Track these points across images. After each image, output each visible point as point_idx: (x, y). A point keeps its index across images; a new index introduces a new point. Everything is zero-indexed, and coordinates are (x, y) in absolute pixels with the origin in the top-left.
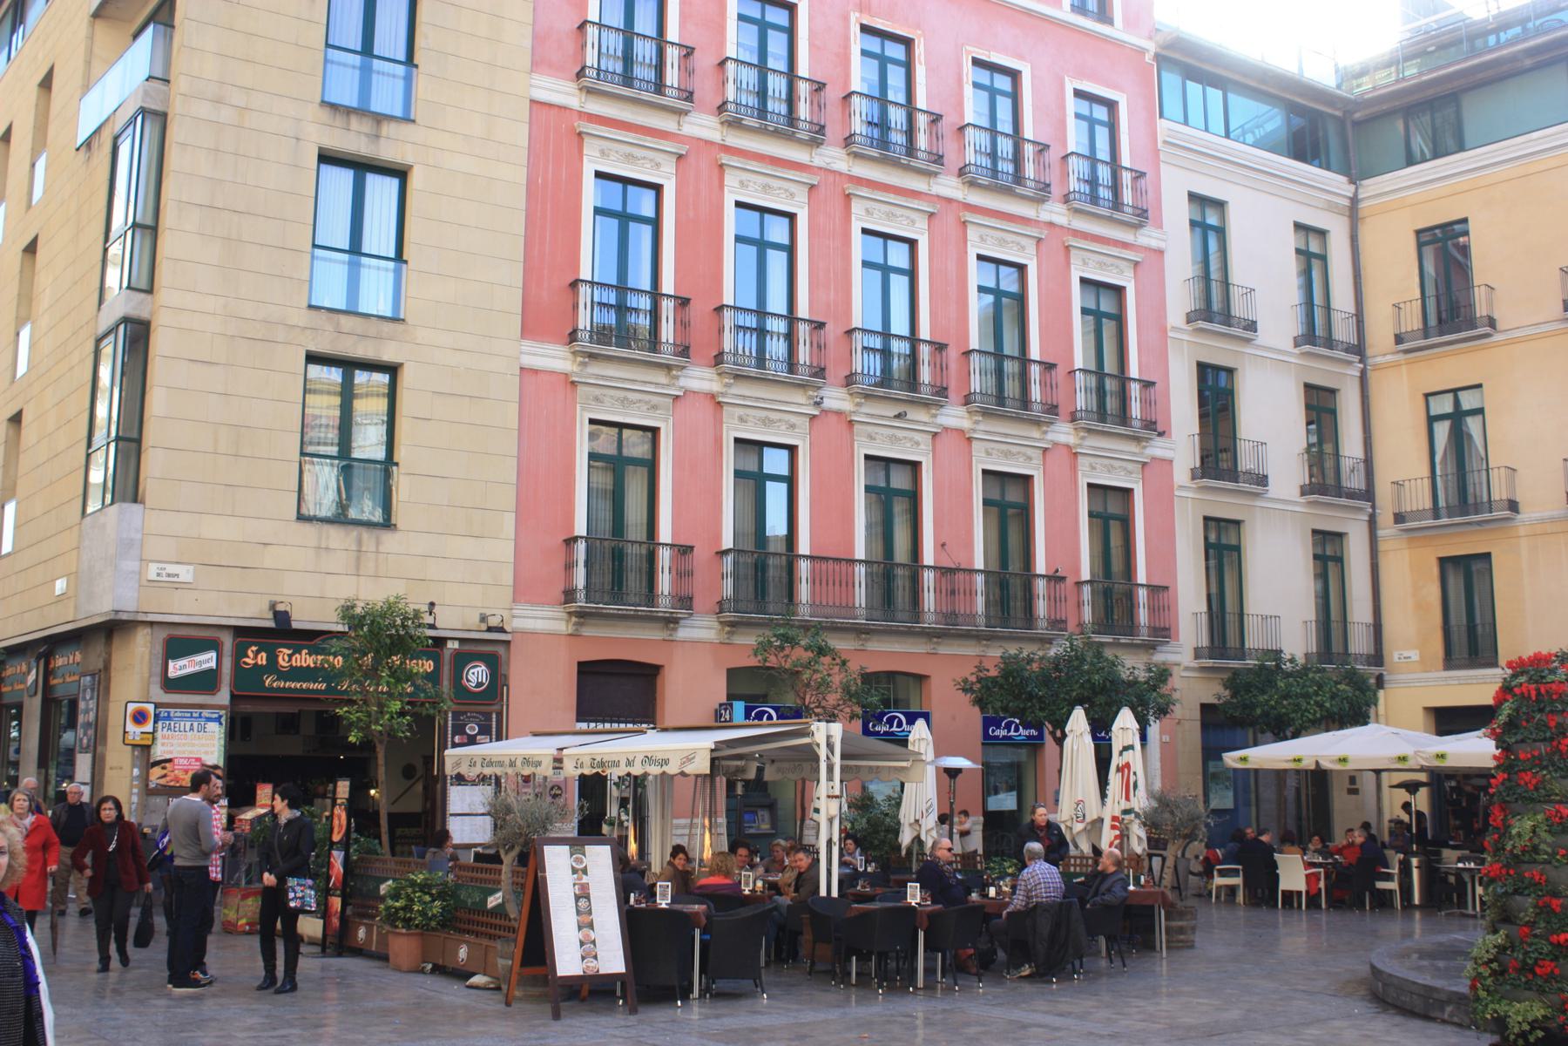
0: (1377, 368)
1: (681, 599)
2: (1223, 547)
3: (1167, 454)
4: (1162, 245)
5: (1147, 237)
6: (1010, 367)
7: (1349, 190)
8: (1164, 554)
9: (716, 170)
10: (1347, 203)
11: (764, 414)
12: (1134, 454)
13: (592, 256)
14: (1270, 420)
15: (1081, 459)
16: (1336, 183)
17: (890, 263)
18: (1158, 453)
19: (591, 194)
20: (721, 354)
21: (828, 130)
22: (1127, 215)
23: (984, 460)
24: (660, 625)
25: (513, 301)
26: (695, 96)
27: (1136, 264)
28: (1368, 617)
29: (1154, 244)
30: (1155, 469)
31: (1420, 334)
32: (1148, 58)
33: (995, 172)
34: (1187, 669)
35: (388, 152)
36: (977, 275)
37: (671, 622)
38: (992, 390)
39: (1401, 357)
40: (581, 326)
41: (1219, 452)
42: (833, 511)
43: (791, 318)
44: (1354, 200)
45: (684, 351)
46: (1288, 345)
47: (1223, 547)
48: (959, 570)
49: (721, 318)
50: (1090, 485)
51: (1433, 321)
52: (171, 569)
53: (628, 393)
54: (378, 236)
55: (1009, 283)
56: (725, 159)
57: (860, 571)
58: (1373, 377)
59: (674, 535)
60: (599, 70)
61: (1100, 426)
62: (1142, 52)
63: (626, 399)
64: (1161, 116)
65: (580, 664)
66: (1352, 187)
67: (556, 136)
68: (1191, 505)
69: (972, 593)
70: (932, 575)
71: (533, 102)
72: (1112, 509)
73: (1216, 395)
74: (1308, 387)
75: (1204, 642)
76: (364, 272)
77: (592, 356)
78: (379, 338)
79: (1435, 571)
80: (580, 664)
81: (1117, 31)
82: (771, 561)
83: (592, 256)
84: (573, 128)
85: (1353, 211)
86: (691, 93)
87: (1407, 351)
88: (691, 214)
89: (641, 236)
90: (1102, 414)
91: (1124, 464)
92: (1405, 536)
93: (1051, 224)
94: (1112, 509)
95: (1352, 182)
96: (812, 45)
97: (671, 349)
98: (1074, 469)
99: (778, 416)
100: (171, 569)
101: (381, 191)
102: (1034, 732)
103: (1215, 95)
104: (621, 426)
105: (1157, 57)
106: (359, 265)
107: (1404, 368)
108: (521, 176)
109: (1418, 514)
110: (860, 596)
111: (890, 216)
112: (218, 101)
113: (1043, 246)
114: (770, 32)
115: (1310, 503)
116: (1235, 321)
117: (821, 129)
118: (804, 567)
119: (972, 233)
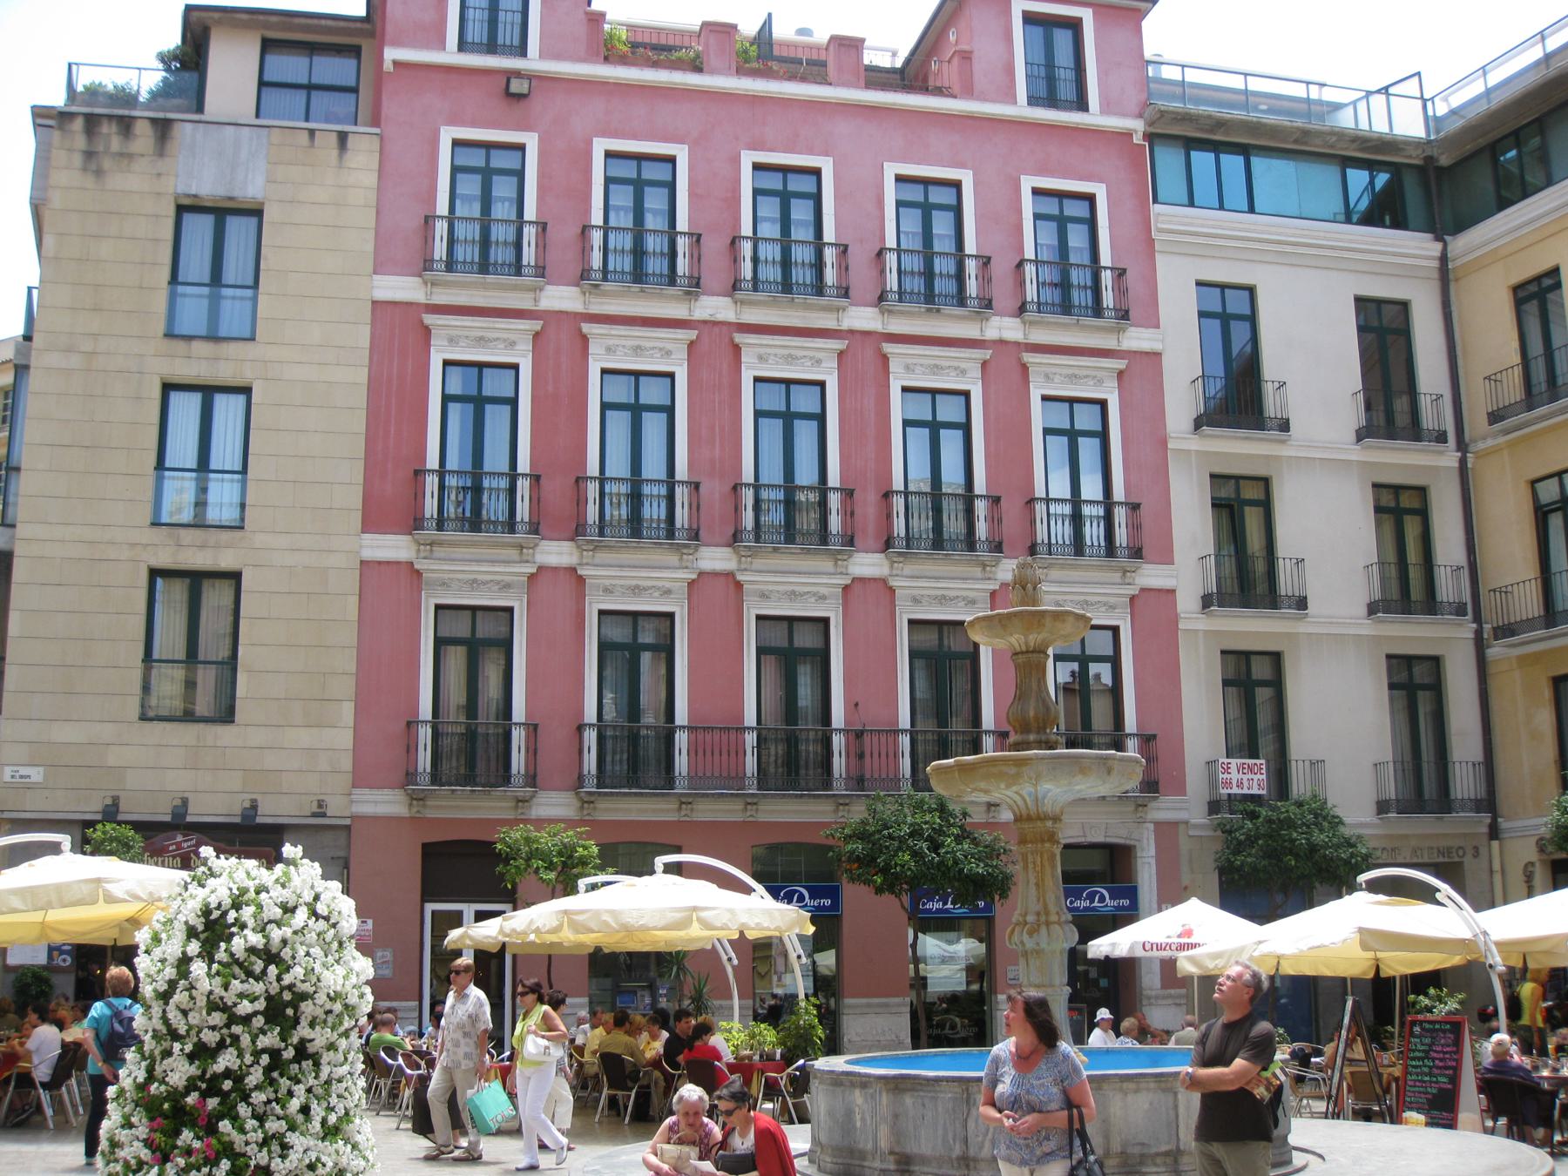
2: (1255, 686)
10: (1436, 264)
13: (438, 439)
14: (1326, 533)
16: (1416, 246)
19: (1038, 417)
25: (355, 498)
26: (851, 293)
28: (1477, 754)
29: (1146, 346)
30: (1154, 608)
32: (1138, 139)
34: (1196, 826)
35: (224, 373)
39: (1502, 440)
41: (1249, 575)
42: (557, 675)
43: (442, 473)
44: (1444, 259)
49: (1032, 512)
52: (24, 771)
53: (476, 573)
54: (225, 452)
60: (1039, 304)
62: (1128, 135)
64: (1155, 201)
65: (424, 846)
66: (1439, 246)
67: (400, 332)
68: (1204, 635)
71: (374, 303)
73: (1241, 506)
76: (166, 482)
78: (217, 546)
79: (1547, 693)
80: (424, 846)
81: (1094, 117)
82: (643, 732)
83: (438, 439)
85: (1445, 274)
88: (550, 388)
89: (805, 433)
93: (1002, 342)
95: (1439, 238)
96: (692, 194)
99: (643, 580)
100: (24, 771)
101: (227, 410)
102: (827, 902)
103: (1233, 164)
105: (1149, 137)
106: (207, 480)
108: (362, 376)
109: (1529, 624)
112: (69, 350)
114: (1070, 226)
116: (1269, 424)
118: (681, 739)
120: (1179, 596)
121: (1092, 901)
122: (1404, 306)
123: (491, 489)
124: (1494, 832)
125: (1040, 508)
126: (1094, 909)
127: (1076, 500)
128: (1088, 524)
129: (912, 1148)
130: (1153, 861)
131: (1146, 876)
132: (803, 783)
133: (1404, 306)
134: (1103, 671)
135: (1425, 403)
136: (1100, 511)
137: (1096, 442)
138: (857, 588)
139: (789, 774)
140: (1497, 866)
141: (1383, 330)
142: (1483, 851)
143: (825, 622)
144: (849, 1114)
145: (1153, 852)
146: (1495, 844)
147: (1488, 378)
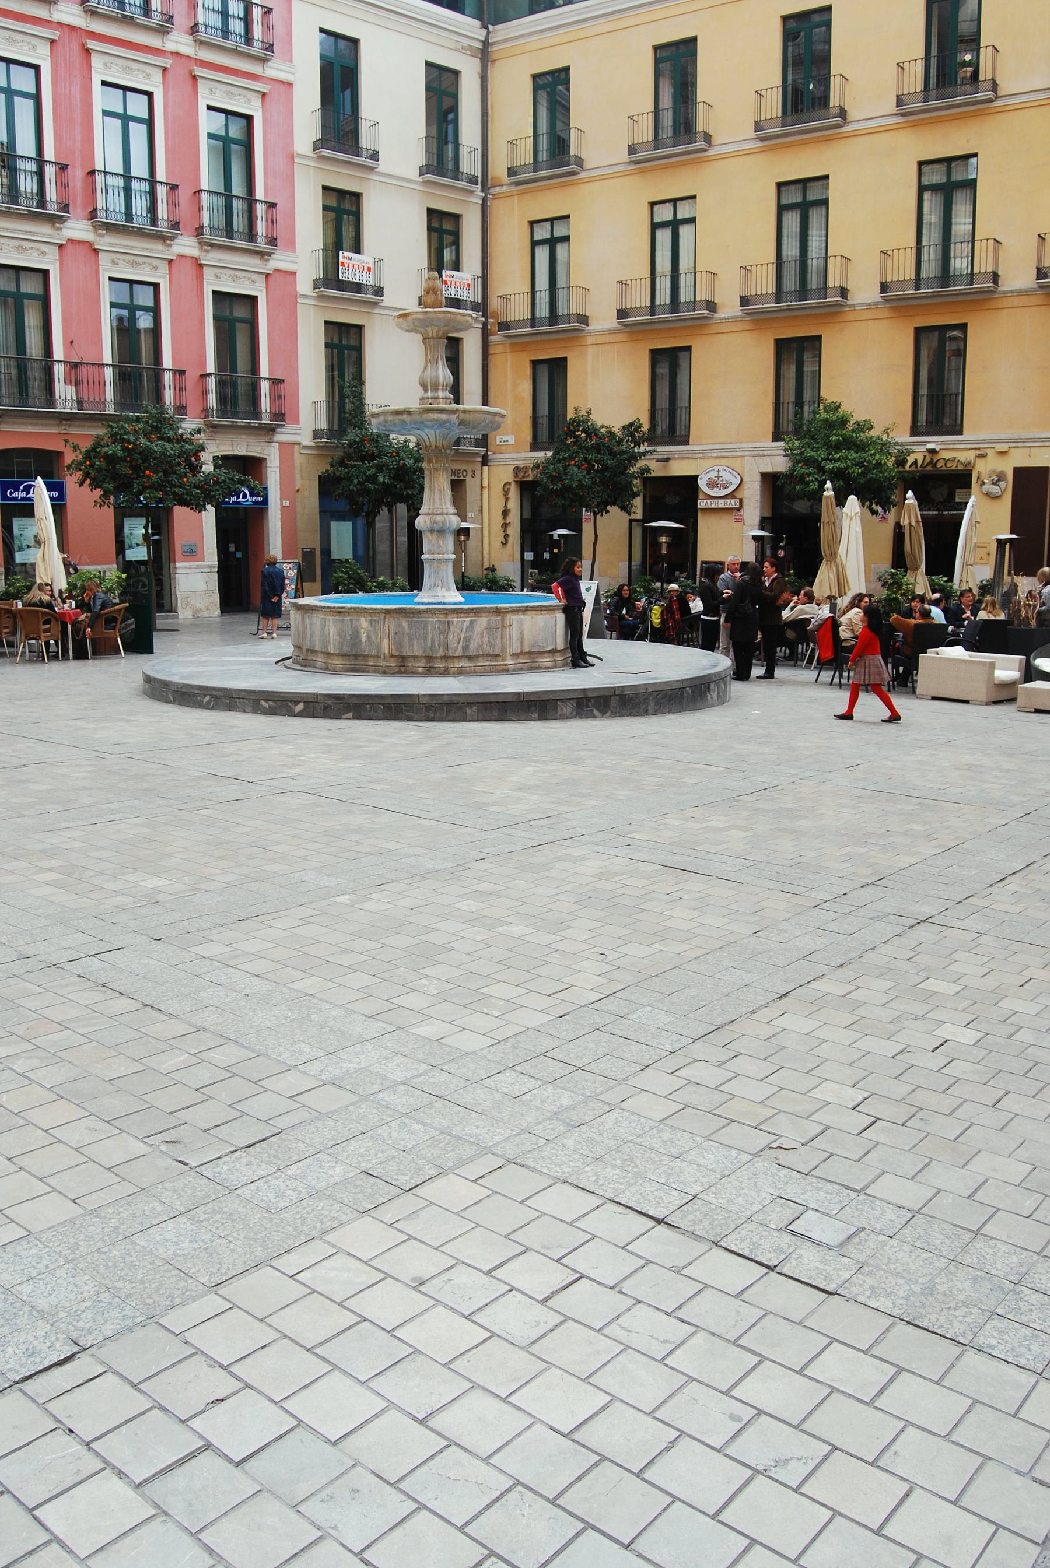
0: (495, 197)
1: (275, 415)
2: (345, 347)
3: (290, 267)
4: (289, 78)
5: (274, 70)
6: (237, 206)
7: (481, 34)
8: (287, 353)
9: (189, 81)
10: (480, 46)
11: (131, 258)
12: (50, 236)
15: (206, 270)
16: (467, 25)
17: (129, 113)
18: (283, 266)
19: (101, 99)
20: (95, 210)
21: (175, 20)
22: (257, 49)
23: (212, 283)
24: (264, 432)
27: (264, 95)
31: (531, 167)
33: (225, 33)
34: (306, 447)
36: (101, 99)
37: (271, 430)
38: (222, 224)
39: (513, 188)
40: (99, 207)
44: (486, 43)
45: (175, 225)
46: (413, 174)
47: (345, 347)
48: (81, 363)
49: (199, 200)
50: (214, 292)
51: (543, 156)
55: (235, 131)
56: (198, 71)
57: (108, 373)
58: (495, 206)
59: (270, 372)
61: (227, 242)
63: (20, 247)
66: (484, 32)
69: (102, 384)
70: (267, 384)
72: (235, 315)
74: (431, 212)
75: (324, 425)
77: (212, 245)
79: (528, 371)
82: (240, 381)
84: (191, 72)
85: (485, 54)
86: (172, 17)
87: (518, 184)
90: (229, 233)
91: (248, 275)
92: (509, 341)
94: (235, 315)
97: (165, 224)
98: (200, 278)
102: (260, 499)
104: (132, 282)
107: (516, 197)
110: (109, 392)
111: (128, 70)
113: (170, 75)
115: (321, 297)
117: (170, 19)
119: (96, 61)
120: (299, 277)
121: (28, 493)
122: (456, 73)
123: (25, 171)
124: (485, 461)
125: (99, 178)
126: (239, 503)
127: (128, 177)
128: (22, 177)
129: (406, 652)
130: (278, 470)
131: (273, 480)
132: (31, 402)
133: (456, 73)
134: (144, 321)
135: (464, 152)
136: (145, 187)
137: (30, 103)
138: (70, 248)
139: (21, 394)
140: (485, 484)
141: (442, 87)
142: (478, 473)
143: (253, 299)
144: (356, 634)
145: (277, 464)
146: (486, 468)
147: (511, 142)
